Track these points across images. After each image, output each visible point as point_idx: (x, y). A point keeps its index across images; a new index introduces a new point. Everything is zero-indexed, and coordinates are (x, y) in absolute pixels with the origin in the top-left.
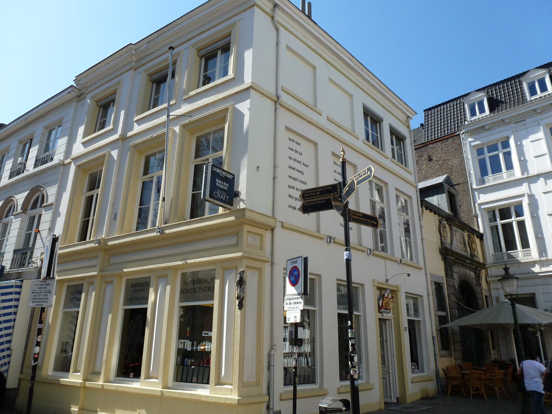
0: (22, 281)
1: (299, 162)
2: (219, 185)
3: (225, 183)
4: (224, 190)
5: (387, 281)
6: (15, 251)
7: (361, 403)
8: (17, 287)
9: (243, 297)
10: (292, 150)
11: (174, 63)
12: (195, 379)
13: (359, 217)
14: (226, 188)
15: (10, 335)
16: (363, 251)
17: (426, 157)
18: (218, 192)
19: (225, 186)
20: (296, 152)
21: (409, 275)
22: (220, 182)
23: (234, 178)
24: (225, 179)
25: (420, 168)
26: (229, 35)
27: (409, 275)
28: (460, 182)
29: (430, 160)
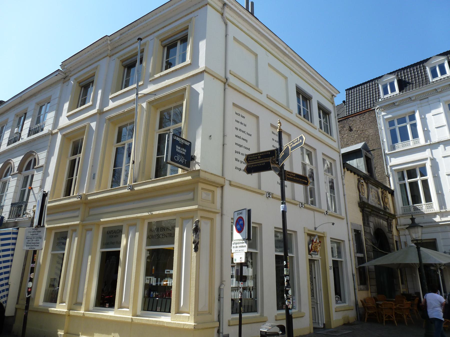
0: (18, 229)
1: (244, 132)
2: (178, 151)
3: (183, 149)
4: (183, 155)
5: (315, 228)
6: (12, 204)
7: (294, 328)
8: (14, 233)
9: (198, 242)
10: (238, 122)
11: (142, 51)
12: (159, 308)
13: (293, 176)
14: (184, 153)
15: (8, 272)
16: (296, 205)
17: (347, 127)
18: (178, 157)
19: (184, 151)
20: (242, 123)
21: (333, 224)
22: (179, 148)
23: (190, 145)
24: (183, 146)
25: (342, 137)
26: (187, 29)
27: (333, 224)
28: (375, 148)
29: (351, 130)
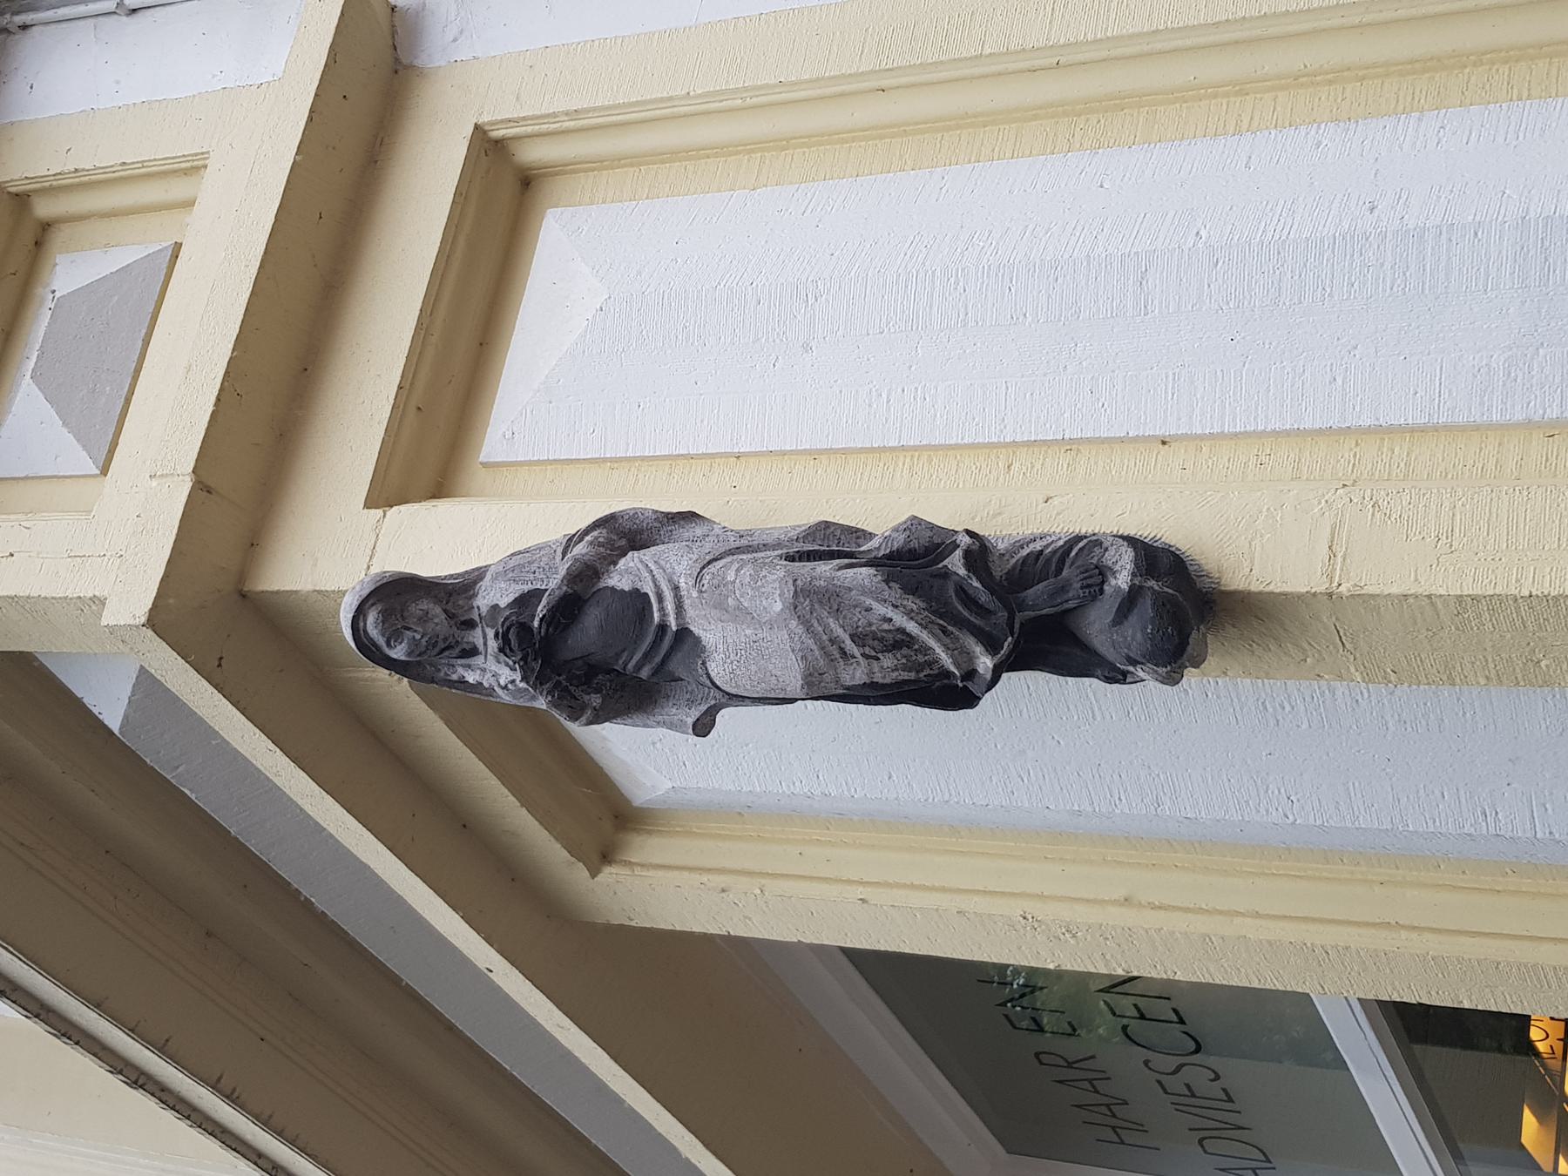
9: (916, 560)
